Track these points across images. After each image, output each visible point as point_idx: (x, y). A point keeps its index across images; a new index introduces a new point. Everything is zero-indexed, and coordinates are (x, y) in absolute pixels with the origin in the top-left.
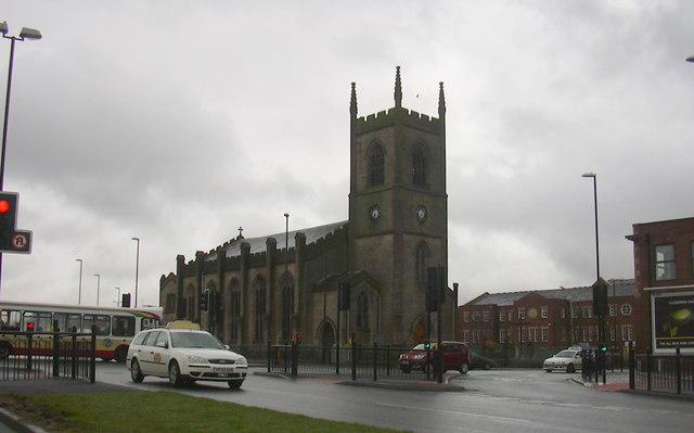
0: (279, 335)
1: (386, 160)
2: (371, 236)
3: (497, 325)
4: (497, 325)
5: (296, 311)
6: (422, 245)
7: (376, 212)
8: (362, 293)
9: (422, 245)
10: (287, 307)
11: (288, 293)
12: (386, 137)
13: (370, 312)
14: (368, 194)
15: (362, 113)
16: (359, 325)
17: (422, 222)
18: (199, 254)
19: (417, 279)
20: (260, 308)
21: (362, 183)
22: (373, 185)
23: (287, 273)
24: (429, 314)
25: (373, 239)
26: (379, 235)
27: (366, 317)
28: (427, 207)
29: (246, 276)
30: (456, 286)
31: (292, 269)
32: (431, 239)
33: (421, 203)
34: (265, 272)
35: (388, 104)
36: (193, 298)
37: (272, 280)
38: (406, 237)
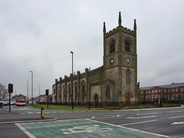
0: (81, 98)
1: (116, 44)
2: (111, 68)
3: (145, 95)
4: (145, 95)
5: (86, 91)
6: (128, 70)
7: (112, 61)
8: (108, 85)
9: (128, 70)
10: (83, 90)
11: (83, 87)
12: (116, 37)
13: (110, 91)
14: (110, 56)
15: (107, 31)
16: (107, 95)
17: (128, 63)
18: (66, 77)
19: (127, 80)
20: (76, 92)
21: (107, 53)
22: (111, 53)
23: (83, 81)
24: (10, 94)
25: (111, 69)
26: (113, 67)
27: (109, 92)
28: (130, 58)
29: (72, 83)
30: (139, 83)
31: (84, 79)
32: (131, 68)
33: (128, 57)
34: (77, 81)
35: (116, 25)
36: (77, 86)
37: (79, 83)
38: (123, 67)
